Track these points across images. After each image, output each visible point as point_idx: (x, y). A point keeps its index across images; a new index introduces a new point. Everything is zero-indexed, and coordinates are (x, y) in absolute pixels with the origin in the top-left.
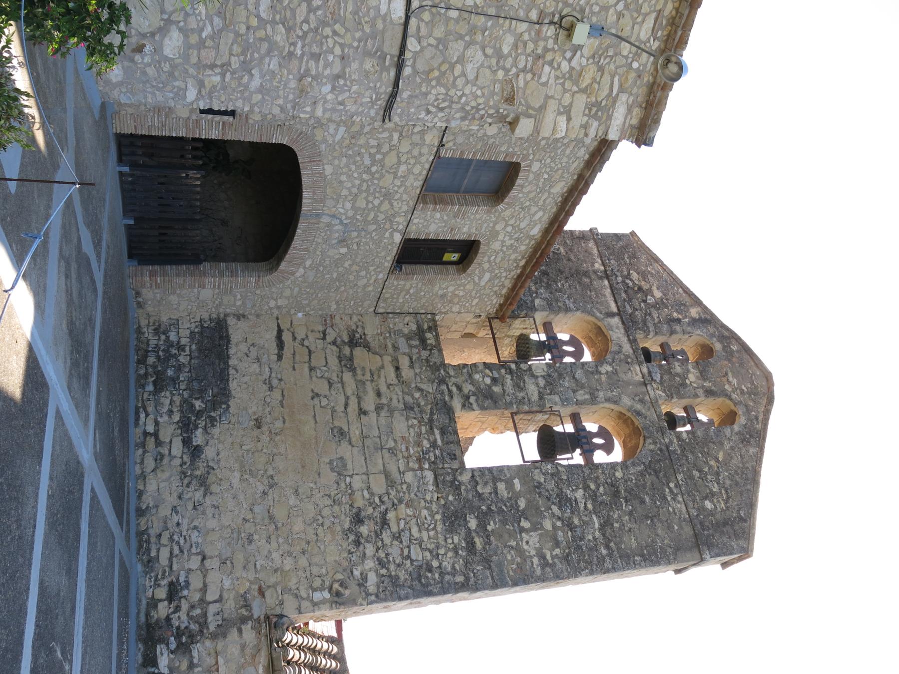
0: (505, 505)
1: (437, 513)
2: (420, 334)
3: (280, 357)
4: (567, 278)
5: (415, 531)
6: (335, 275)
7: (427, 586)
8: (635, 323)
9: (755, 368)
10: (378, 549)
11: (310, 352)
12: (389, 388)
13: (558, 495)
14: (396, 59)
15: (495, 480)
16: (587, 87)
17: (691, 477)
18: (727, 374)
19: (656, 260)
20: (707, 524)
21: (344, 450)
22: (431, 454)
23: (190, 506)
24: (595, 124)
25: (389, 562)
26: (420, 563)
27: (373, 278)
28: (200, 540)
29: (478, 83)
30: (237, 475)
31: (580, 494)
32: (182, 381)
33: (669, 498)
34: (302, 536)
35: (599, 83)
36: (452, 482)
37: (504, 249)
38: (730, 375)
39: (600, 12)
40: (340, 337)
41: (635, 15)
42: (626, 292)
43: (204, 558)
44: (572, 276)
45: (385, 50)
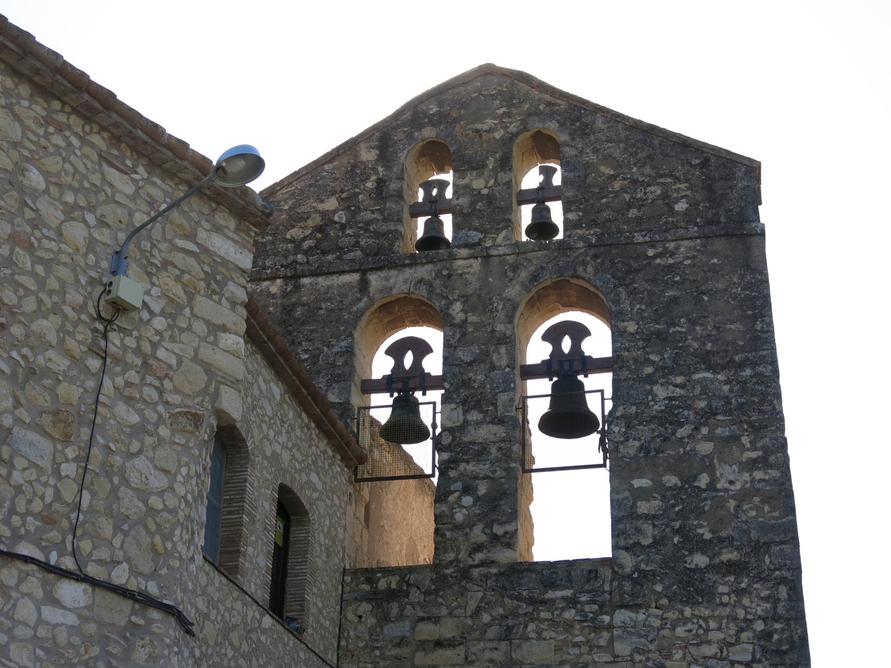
0: (674, 506)
1: (681, 612)
2: (381, 599)
4: (293, 342)
7: (793, 642)
8: (378, 252)
9: (470, 87)
12: (472, 662)
13: (661, 425)
14: (137, 606)
15: (633, 515)
16: (185, 292)
17: (638, 221)
18: (477, 131)
20: (709, 215)
22: (587, 608)
24: (231, 287)
26: (758, 649)
29: (173, 472)
31: (661, 392)
33: (671, 261)
35: (183, 272)
36: (635, 582)
38: (479, 126)
39: (95, 253)
41: (102, 197)
42: (324, 253)
44: (290, 333)
45: (122, 622)
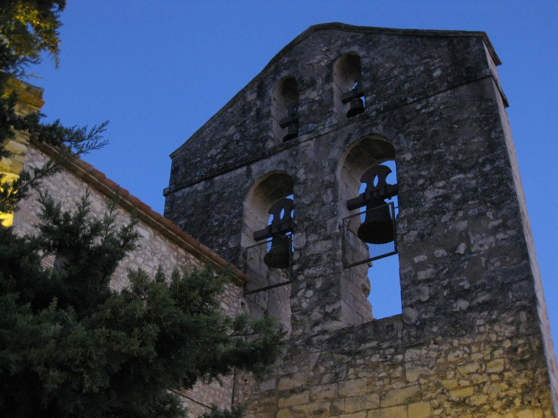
0: (442, 270)
7: (532, 352)
10: (493, 409)
25: (506, 396)
33: (432, 109)
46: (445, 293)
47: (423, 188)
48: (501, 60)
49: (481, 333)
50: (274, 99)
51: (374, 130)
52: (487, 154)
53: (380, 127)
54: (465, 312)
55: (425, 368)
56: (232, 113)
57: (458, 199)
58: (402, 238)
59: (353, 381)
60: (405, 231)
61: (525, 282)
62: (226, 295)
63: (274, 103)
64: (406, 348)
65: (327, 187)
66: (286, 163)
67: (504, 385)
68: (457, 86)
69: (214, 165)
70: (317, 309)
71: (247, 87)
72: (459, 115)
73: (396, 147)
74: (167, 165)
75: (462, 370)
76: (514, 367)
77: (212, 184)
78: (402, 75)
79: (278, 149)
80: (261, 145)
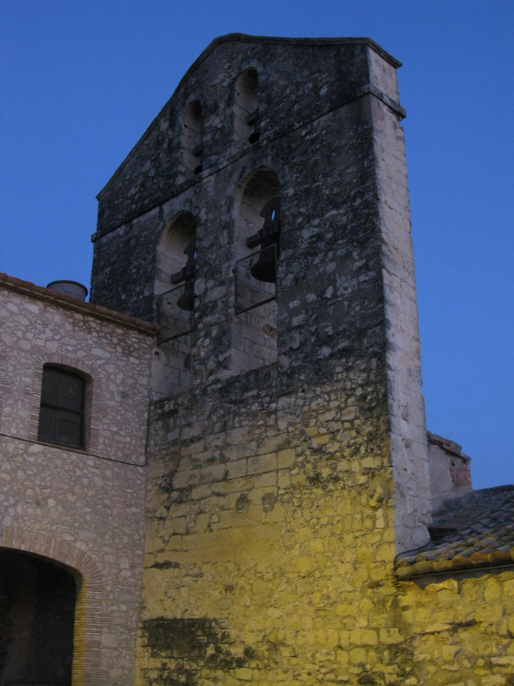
0: (311, 316)
3: (177, 566)
5: (329, 416)
6: (88, 510)
7: (378, 399)
10: (343, 457)
11: (175, 534)
19: (121, 169)
21: (255, 497)
23: (294, 661)
25: (355, 444)
27: (92, 470)
28: (324, 651)
30: (271, 611)
32: (191, 666)
33: (315, 135)
34: (326, 541)
37: (57, 337)
40: (164, 502)
43: (340, 647)
46: (312, 340)
47: (301, 227)
48: (401, 60)
49: (338, 381)
50: (186, 126)
51: (265, 163)
52: (359, 186)
53: (270, 158)
54: (327, 359)
55: (293, 416)
56: (148, 145)
57: (330, 239)
58: (281, 282)
59: (237, 429)
60: (284, 275)
61: (378, 327)
62: (135, 349)
63: (185, 131)
64: (278, 397)
65: (224, 227)
66: (191, 202)
67: (354, 433)
68: (338, 107)
69: (133, 206)
70: (213, 358)
71: (160, 115)
72: (337, 142)
73: (282, 182)
74: (94, 207)
75: (322, 418)
76: (363, 415)
77: (131, 227)
78: (293, 94)
79: (184, 187)
80: (172, 181)
